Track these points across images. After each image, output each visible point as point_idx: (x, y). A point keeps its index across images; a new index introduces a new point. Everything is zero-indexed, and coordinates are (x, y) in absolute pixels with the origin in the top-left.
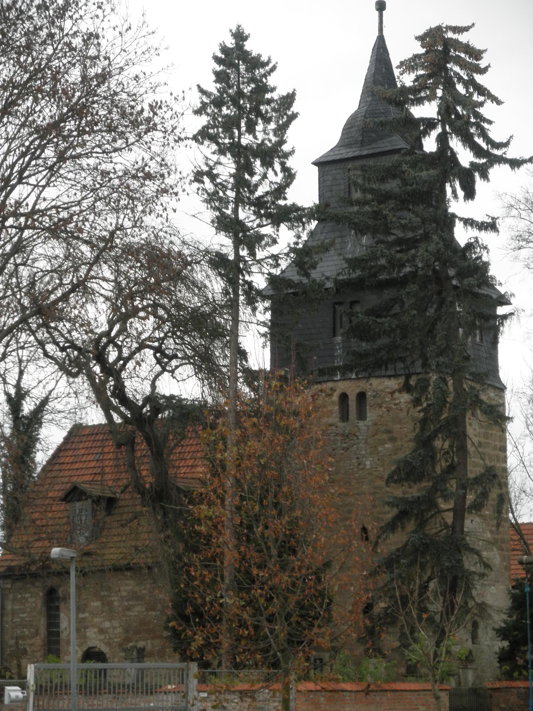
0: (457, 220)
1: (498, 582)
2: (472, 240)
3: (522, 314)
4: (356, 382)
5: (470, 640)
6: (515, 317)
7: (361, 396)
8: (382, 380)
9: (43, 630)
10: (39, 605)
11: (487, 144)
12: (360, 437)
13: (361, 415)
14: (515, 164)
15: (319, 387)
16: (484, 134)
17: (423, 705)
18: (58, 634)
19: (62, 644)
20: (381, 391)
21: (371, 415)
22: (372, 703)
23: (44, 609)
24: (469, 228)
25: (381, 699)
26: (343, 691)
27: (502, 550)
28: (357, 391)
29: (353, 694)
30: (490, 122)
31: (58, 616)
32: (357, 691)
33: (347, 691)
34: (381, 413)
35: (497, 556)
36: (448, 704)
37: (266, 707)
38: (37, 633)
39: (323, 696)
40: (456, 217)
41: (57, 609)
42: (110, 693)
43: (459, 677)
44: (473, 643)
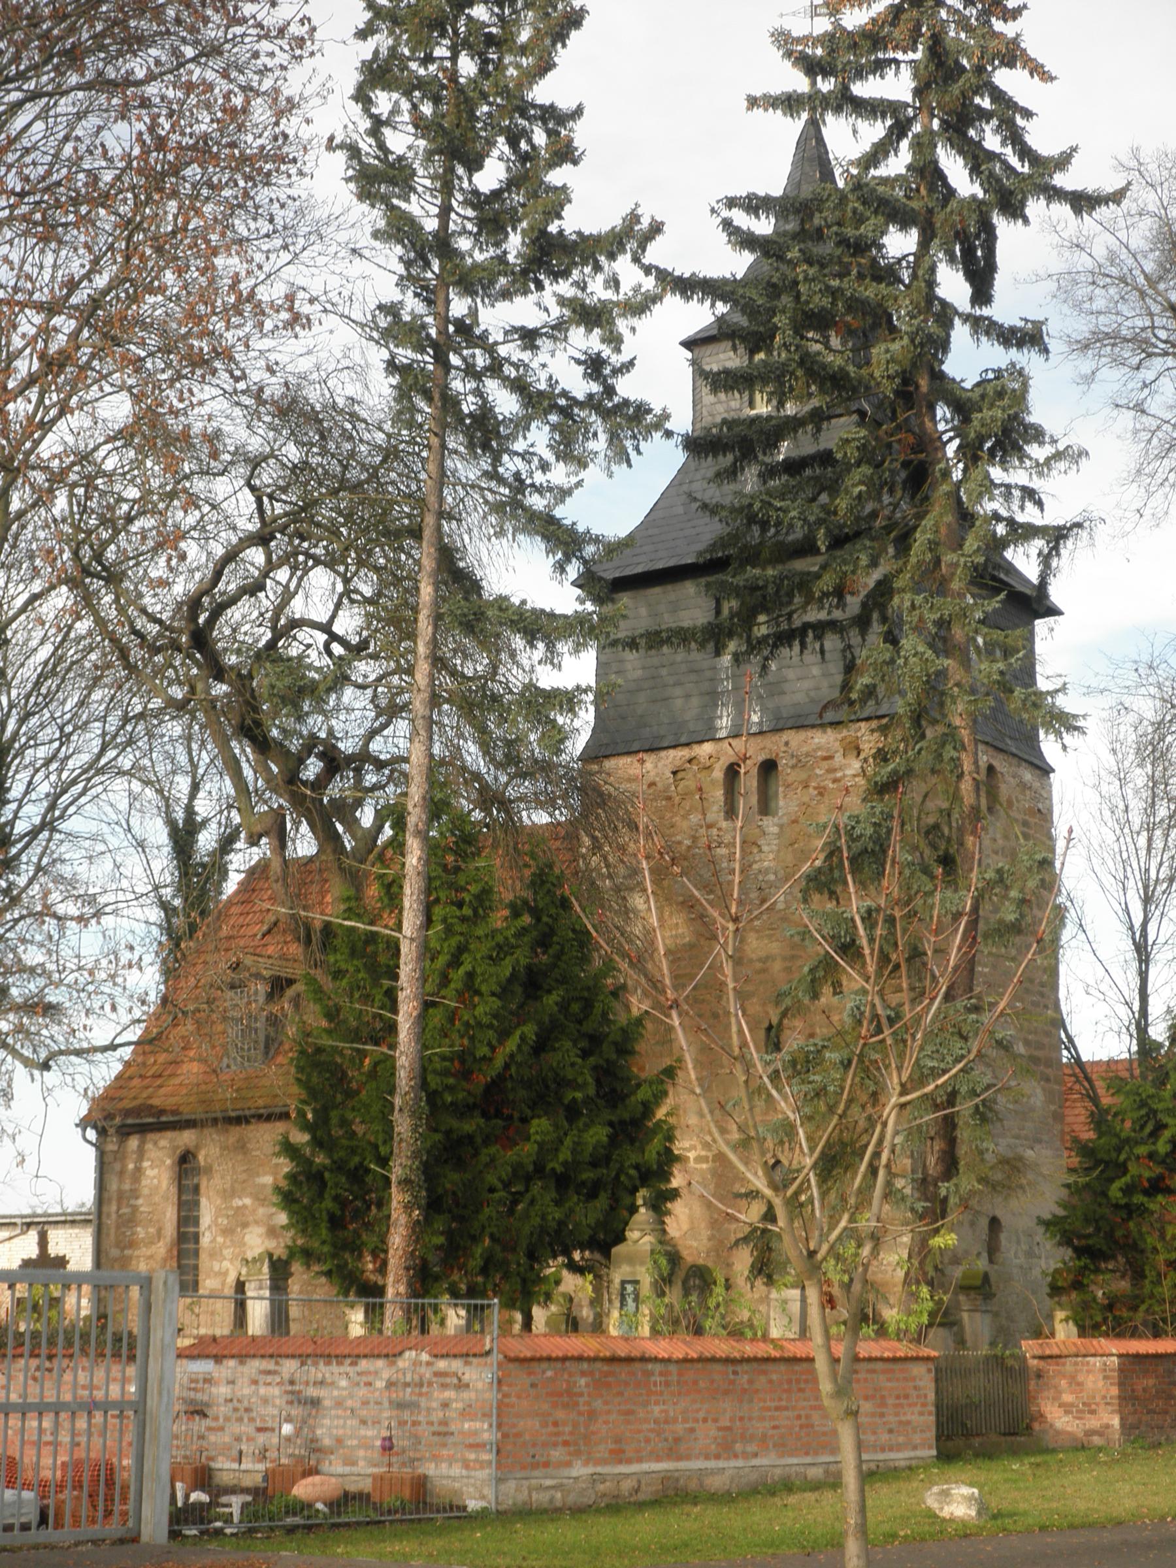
0: (957, 321)
1: (1039, 1141)
2: (991, 375)
3: (1101, 531)
4: (759, 739)
5: (985, 1255)
6: (1084, 534)
7: (769, 768)
8: (810, 733)
9: (170, 1230)
10: (165, 1184)
11: (1021, 160)
12: (765, 848)
13: (765, 807)
14: (1082, 202)
15: (684, 753)
16: (1015, 138)
17: (866, 1398)
18: (196, 1238)
19: (203, 1256)
20: (807, 755)
21: (786, 804)
22: (726, 1392)
23: (174, 1190)
24: (984, 339)
25: (750, 1382)
26: (644, 1359)
27: (1048, 1080)
28: (761, 758)
29: (673, 1368)
30: (1028, 114)
31: (197, 1204)
32: (686, 1360)
33: (656, 1359)
34: (806, 799)
35: (1039, 1091)
36: (932, 1396)
37: (423, 1404)
38: (159, 1234)
39: (583, 1374)
40: (956, 312)
41: (196, 1189)
42: (34, 1355)
43: (962, 1328)
44: (991, 1261)
